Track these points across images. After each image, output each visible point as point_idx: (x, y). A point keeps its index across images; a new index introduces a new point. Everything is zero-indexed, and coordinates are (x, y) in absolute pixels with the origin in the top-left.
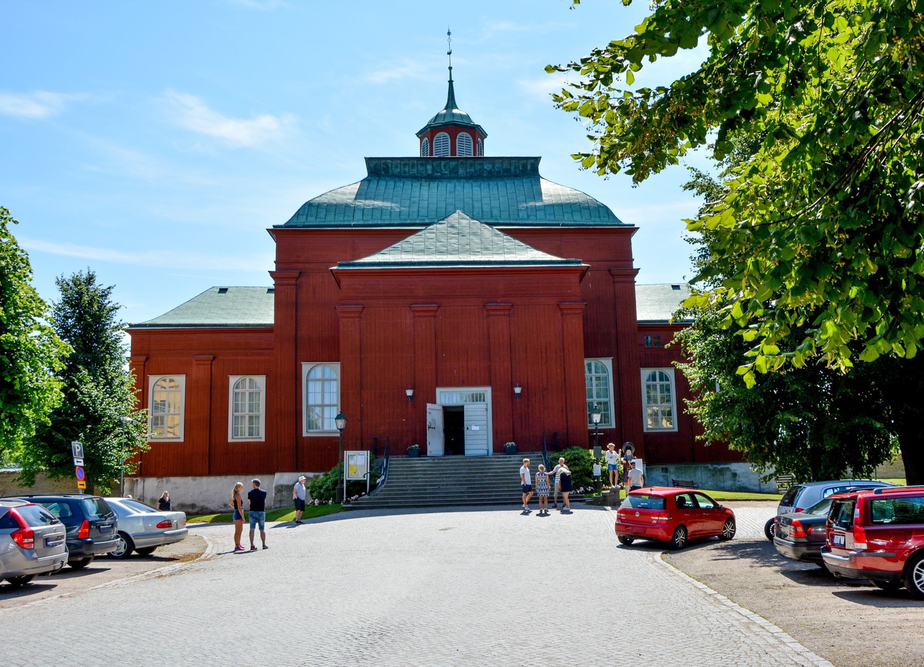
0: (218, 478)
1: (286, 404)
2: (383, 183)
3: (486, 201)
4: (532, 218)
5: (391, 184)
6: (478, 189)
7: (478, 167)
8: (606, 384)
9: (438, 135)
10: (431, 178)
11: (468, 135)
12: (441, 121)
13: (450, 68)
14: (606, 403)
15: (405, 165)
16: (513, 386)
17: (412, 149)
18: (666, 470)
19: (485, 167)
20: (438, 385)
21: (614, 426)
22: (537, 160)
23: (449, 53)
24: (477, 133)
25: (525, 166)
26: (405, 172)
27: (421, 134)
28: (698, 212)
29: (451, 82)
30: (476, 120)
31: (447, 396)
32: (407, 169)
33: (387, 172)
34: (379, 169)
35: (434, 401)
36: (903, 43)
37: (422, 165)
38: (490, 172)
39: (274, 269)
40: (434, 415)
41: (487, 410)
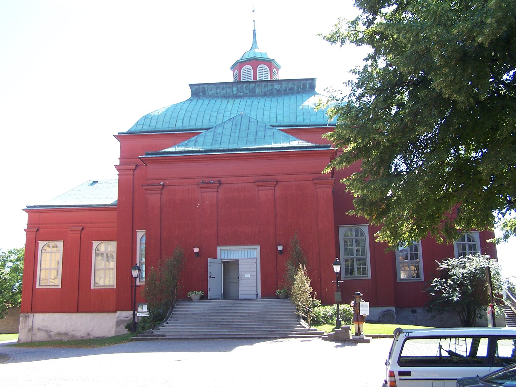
0: (84, 315)
2: (200, 101)
5: (207, 101)
7: (270, 88)
9: (244, 68)
11: (266, 67)
12: (246, 57)
13: (254, 21)
14: (364, 259)
15: (217, 88)
16: (277, 245)
17: (228, 77)
18: (414, 311)
19: (276, 87)
20: (219, 244)
21: (370, 277)
22: (313, 80)
23: (253, 11)
24: (269, 63)
25: (304, 85)
26: (217, 93)
27: (233, 68)
29: (254, 31)
30: (270, 57)
31: (226, 253)
32: (218, 91)
33: (204, 92)
34: (199, 91)
35: (214, 256)
37: (229, 87)
38: (279, 91)
40: (214, 268)
41: (256, 263)
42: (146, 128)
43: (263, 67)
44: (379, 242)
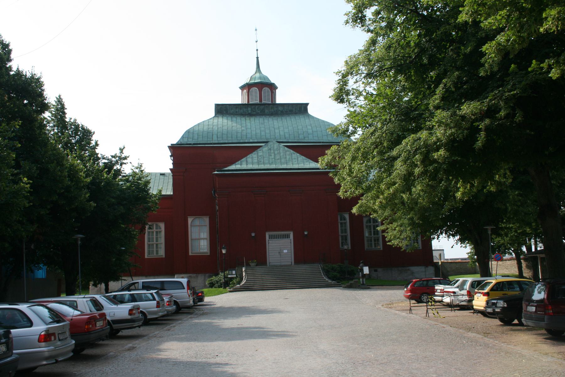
1: (178, 238)
3: (281, 129)
4: (306, 138)
6: (276, 121)
7: (275, 109)
8: (346, 226)
9: (252, 89)
10: (250, 115)
13: (257, 50)
15: (236, 108)
17: (236, 98)
24: (272, 87)
25: (300, 108)
27: (242, 88)
28: (343, 68)
29: (257, 58)
30: (273, 81)
32: (237, 110)
34: (222, 110)
36: (504, 223)
38: (282, 111)
39: (172, 167)
42: (191, 141)
43: (266, 89)
44: (551, 77)
